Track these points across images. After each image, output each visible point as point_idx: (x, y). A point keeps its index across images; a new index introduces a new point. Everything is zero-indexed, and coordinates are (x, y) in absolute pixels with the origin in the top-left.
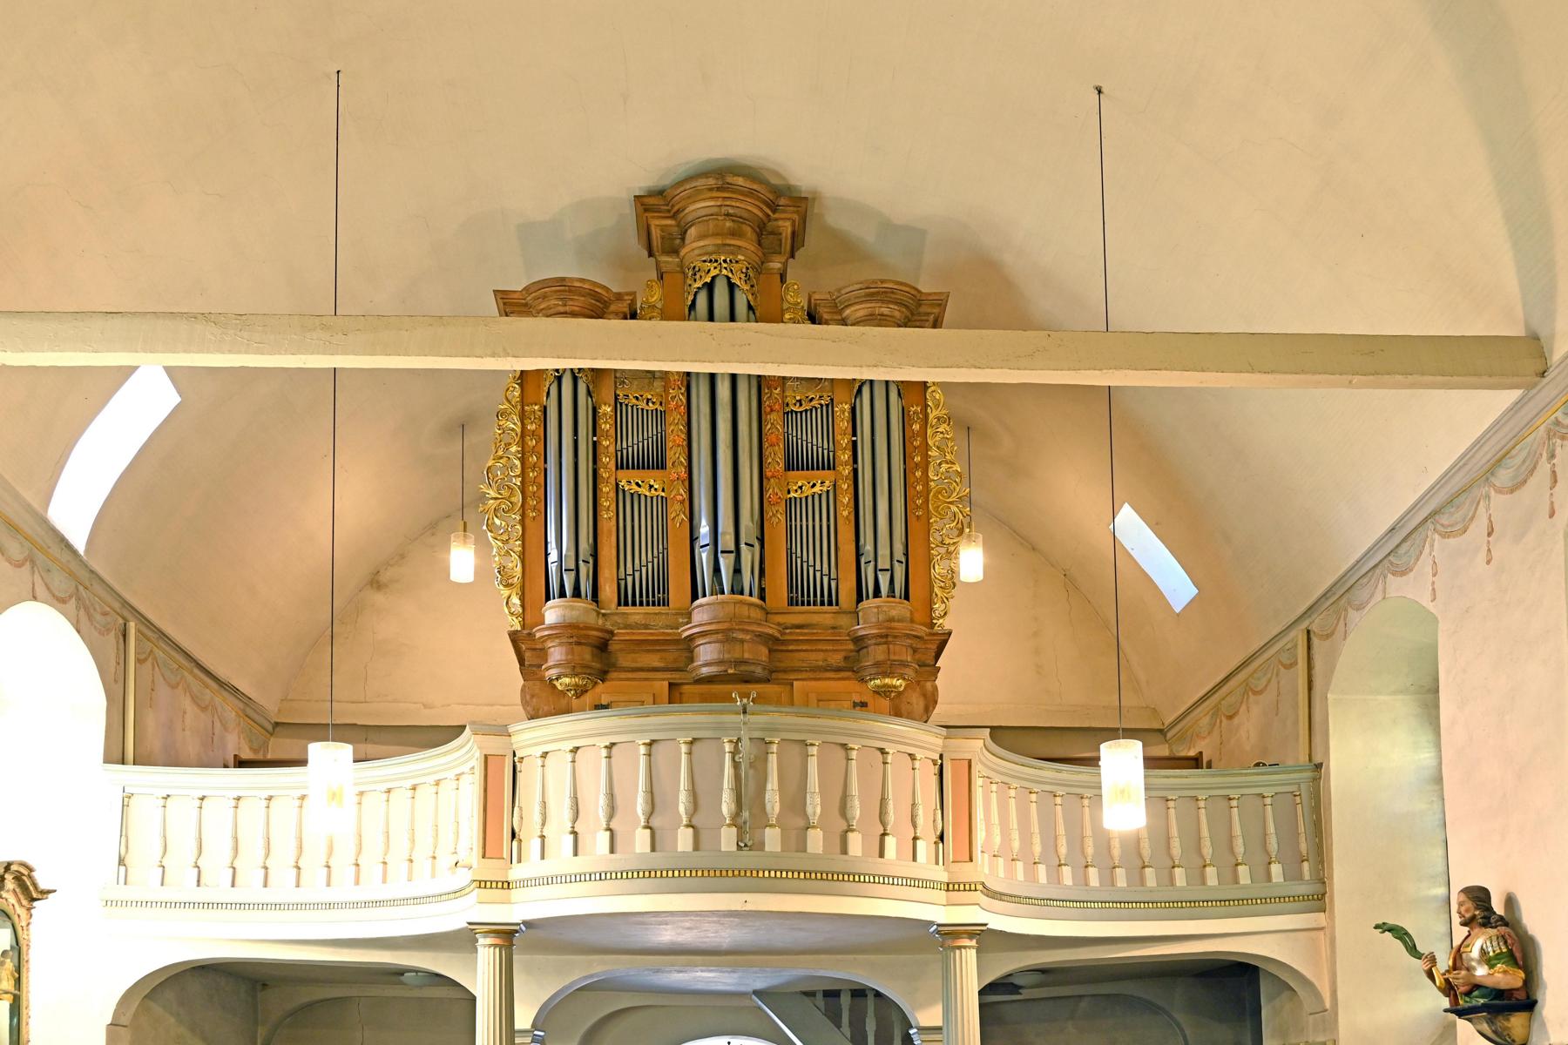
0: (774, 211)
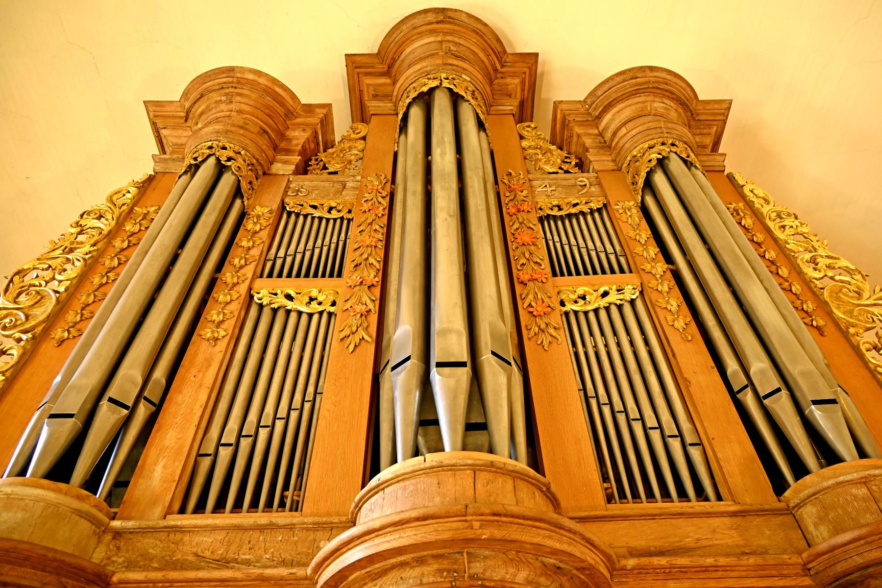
0: (502, 67)
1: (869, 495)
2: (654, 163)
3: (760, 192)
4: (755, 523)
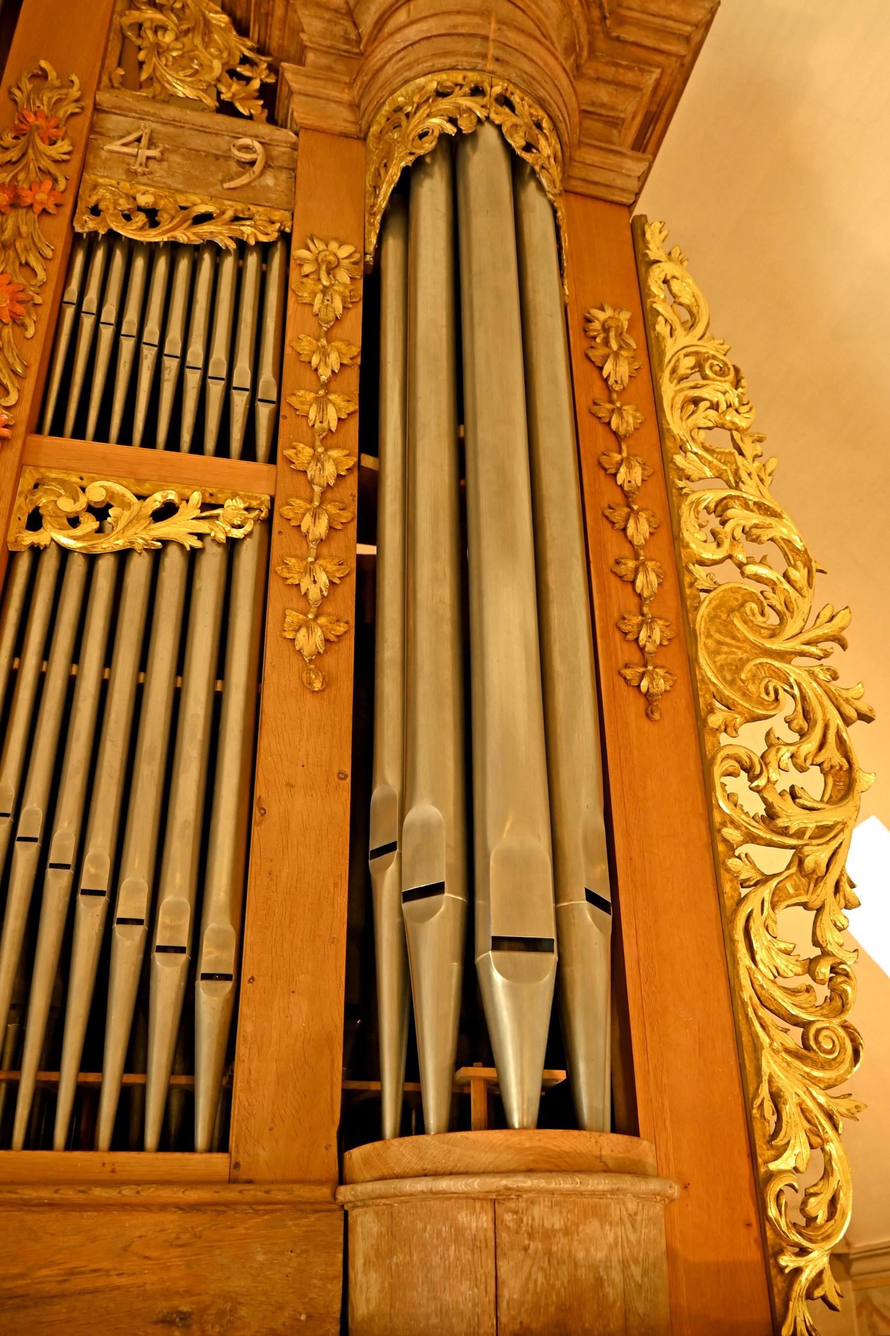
1: (491, 1234)
2: (429, 145)
3: (685, 289)
4: (241, 1230)
